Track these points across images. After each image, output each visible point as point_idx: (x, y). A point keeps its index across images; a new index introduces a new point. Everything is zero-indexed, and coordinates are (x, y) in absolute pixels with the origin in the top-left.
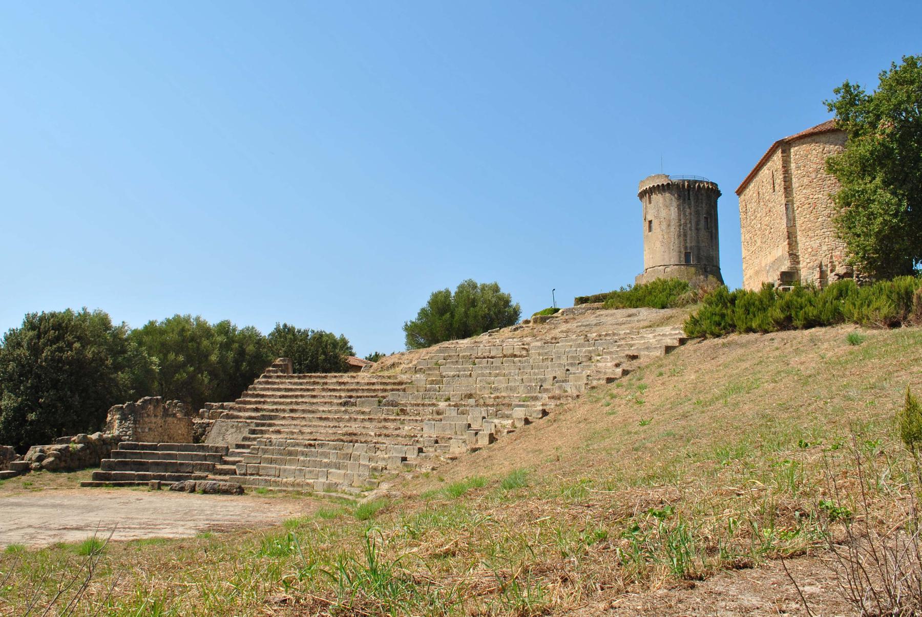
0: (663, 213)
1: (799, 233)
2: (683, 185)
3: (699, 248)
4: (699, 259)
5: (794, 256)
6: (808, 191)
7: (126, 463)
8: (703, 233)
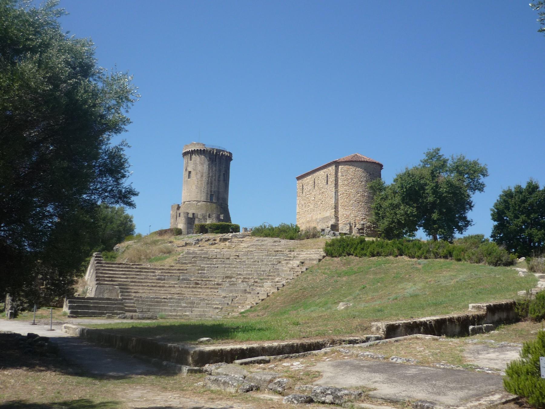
0: (199, 168)
1: (340, 207)
2: (213, 152)
3: (219, 192)
4: (218, 199)
5: (337, 218)
6: (347, 188)
7: (80, 306)
8: (222, 183)
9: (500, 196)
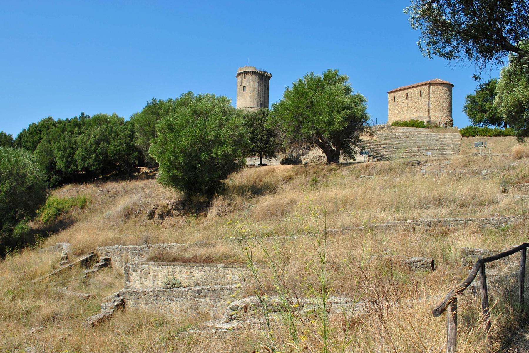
0: (252, 84)
8: (266, 94)
9: (170, 101)
